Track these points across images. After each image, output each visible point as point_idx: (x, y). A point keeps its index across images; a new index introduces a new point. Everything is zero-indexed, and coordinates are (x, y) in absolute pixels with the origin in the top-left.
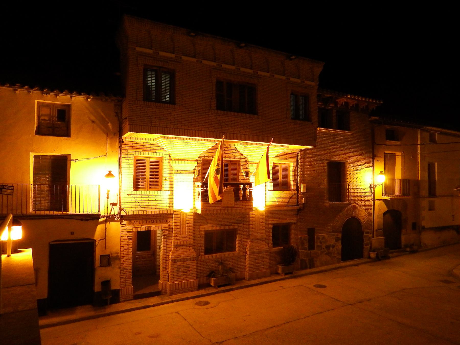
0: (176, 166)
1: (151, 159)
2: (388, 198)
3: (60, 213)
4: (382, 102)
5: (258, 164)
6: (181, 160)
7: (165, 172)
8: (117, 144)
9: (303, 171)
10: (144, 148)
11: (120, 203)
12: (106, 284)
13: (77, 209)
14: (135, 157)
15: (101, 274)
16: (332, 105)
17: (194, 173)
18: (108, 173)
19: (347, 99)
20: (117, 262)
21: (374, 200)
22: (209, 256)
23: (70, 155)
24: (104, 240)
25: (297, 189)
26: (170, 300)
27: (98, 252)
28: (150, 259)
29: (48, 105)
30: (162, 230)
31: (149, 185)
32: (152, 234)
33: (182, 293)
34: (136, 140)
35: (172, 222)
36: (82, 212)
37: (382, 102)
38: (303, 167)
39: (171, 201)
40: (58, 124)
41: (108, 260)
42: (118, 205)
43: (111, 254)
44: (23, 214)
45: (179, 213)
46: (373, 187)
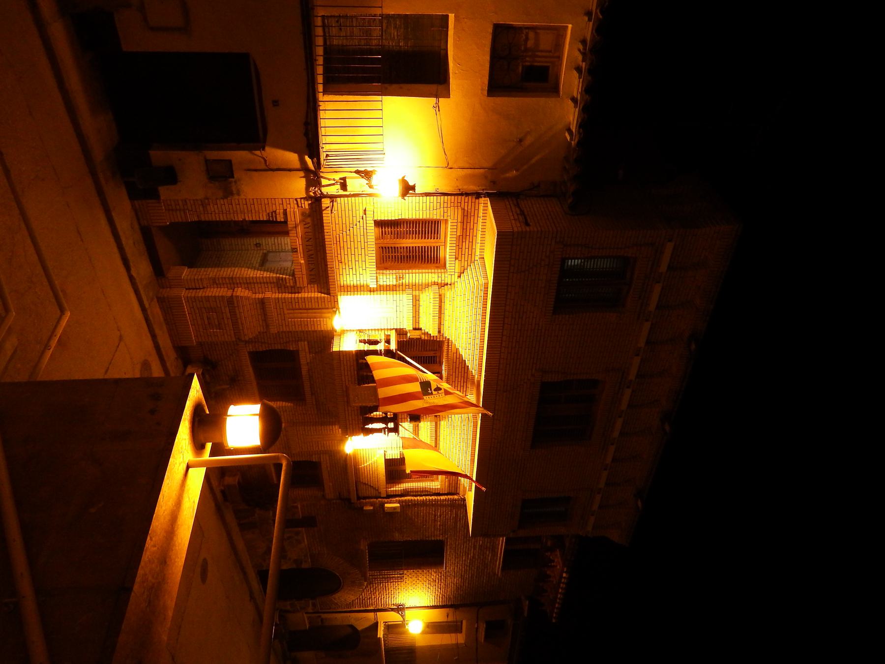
0: (428, 299)
1: (442, 248)
2: (381, 634)
3: (320, 70)
4: (554, 621)
5: (436, 447)
6: (440, 307)
7: (414, 276)
8: (472, 188)
9: (424, 504)
10: (465, 235)
12: (171, 176)
13: (328, 114)
14: (446, 221)
15: (192, 165)
16: (549, 544)
17: (415, 329)
18: (411, 184)
19: (559, 571)
21: (375, 611)
22: (246, 361)
23: (447, 95)
24: (264, 167)
25: (390, 496)
26: (147, 306)
27: (239, 156)
29: (558, 46)
30: (293, 275)
31: (387, 246)
33: (165, 320)
34: (480, 224)
36: (322, 123)
37: (554, 621)
38: (433, 505)
40: (515, 69)
41: (223, 176)
42: (342, 192)
43: (235, 182)
44: (313, 9)
45: (333, 306)
46: (400, 609)
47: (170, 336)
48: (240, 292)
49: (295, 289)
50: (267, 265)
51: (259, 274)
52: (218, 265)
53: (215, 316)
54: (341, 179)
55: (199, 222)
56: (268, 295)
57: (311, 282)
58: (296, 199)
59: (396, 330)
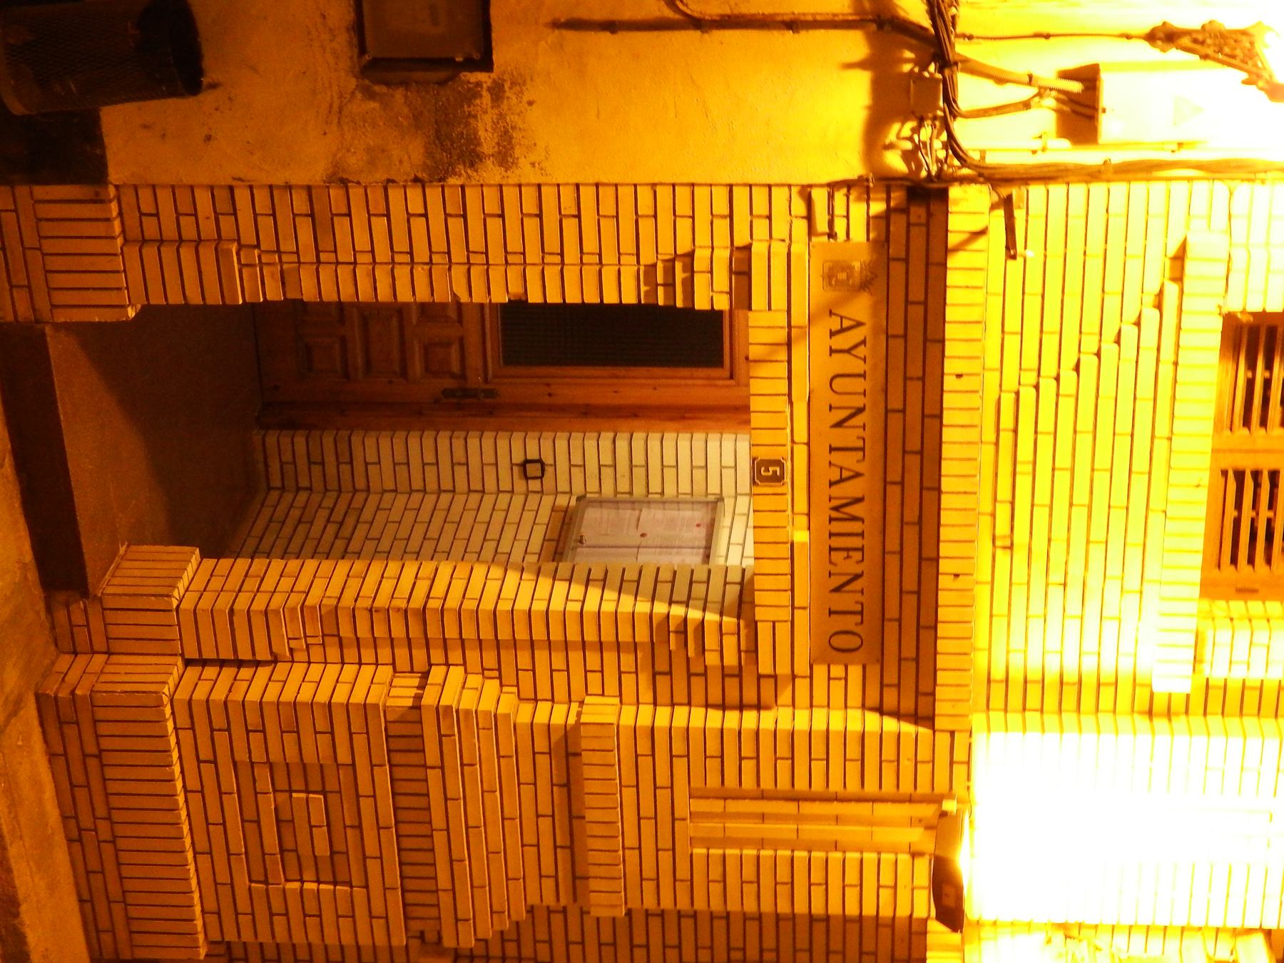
11: (1092, 175)
20: (410, 153)
28: (417, 366)
30: (743, 603)
32: (691, 385)
33: (69, 817)
35: (831, 712)
39: (1068, 696)
42: (1065, 152)
43: (497, 92)
47: (85, 901)
48: (460, 689)
49: (745, 685)
50: (584, 560)
51: (559, 596)
52: (340, 543)
53: (318, 816)
54: (1066, 75)
55: (296, 309)
56: (600, 710)
57: (834, 649)
58: (806, 193)
59: (1268, 933)
